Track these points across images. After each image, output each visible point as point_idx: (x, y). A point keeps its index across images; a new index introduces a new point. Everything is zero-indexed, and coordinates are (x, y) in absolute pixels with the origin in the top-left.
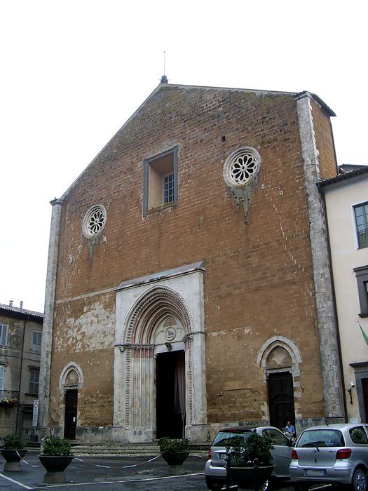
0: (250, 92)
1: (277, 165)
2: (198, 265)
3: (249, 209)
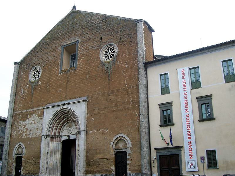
3: (111, 73)
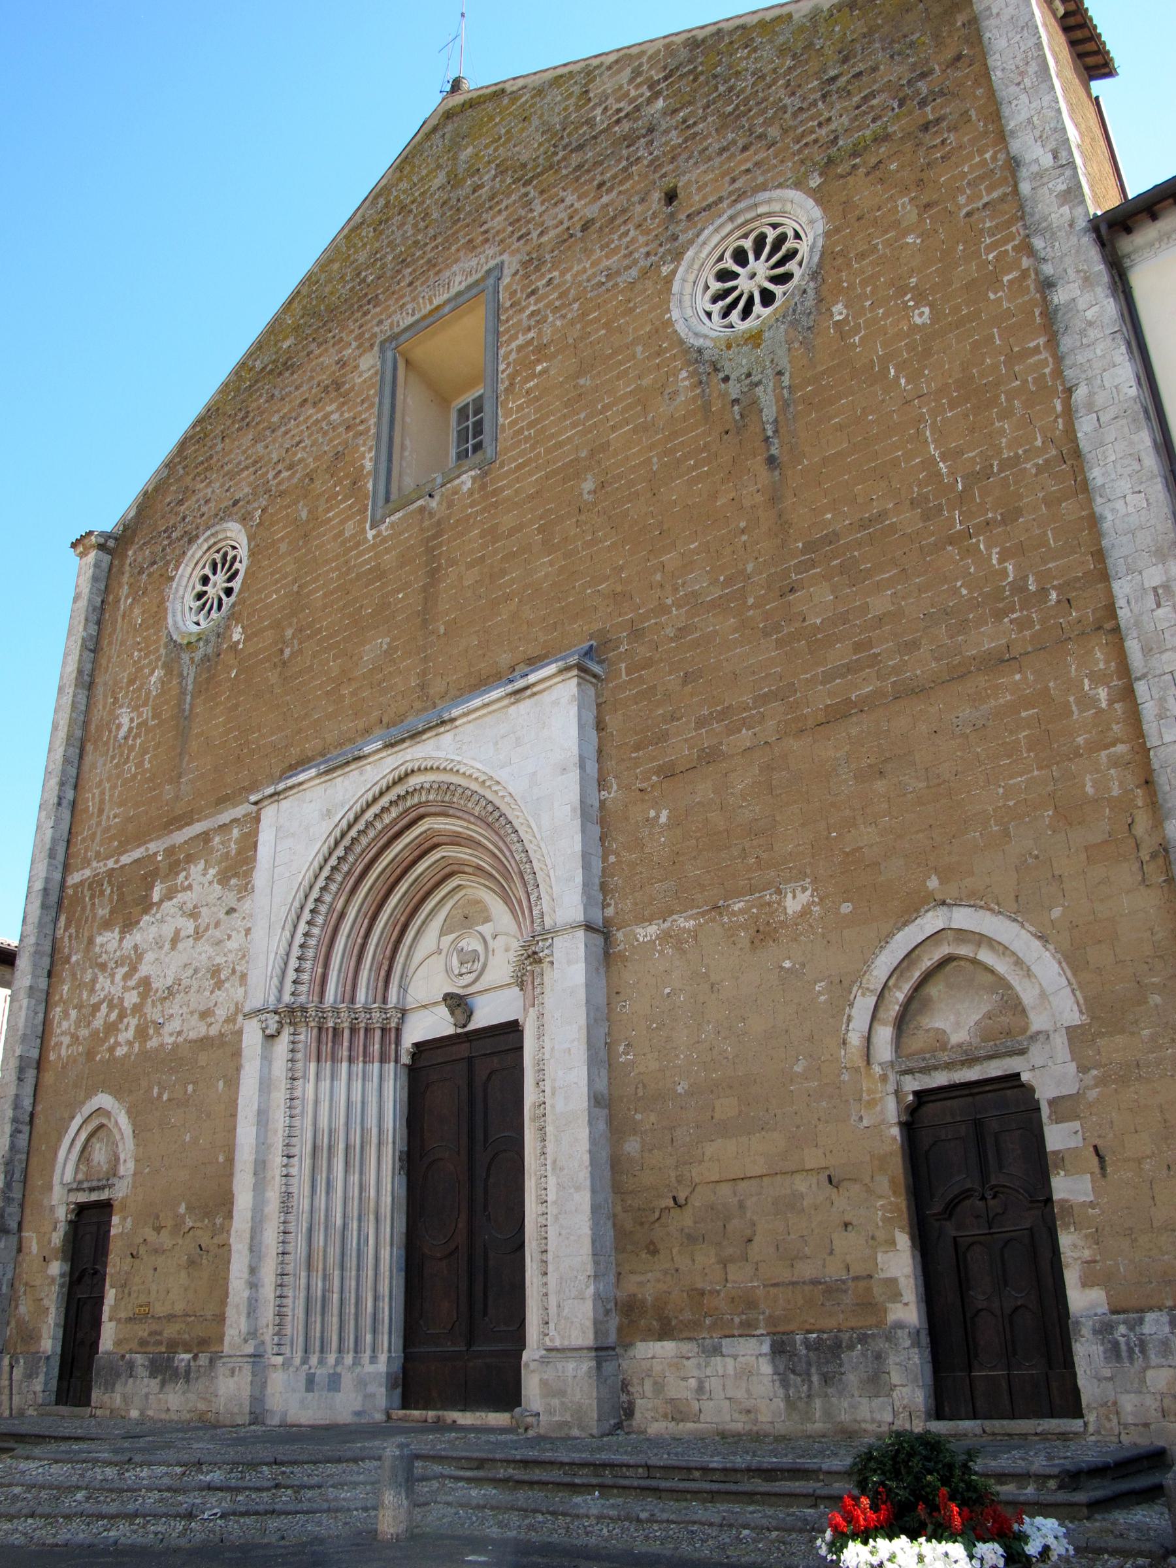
0: (769, 16)
1: (897, 223)
2: (573, 660)
3: (784, 405)
